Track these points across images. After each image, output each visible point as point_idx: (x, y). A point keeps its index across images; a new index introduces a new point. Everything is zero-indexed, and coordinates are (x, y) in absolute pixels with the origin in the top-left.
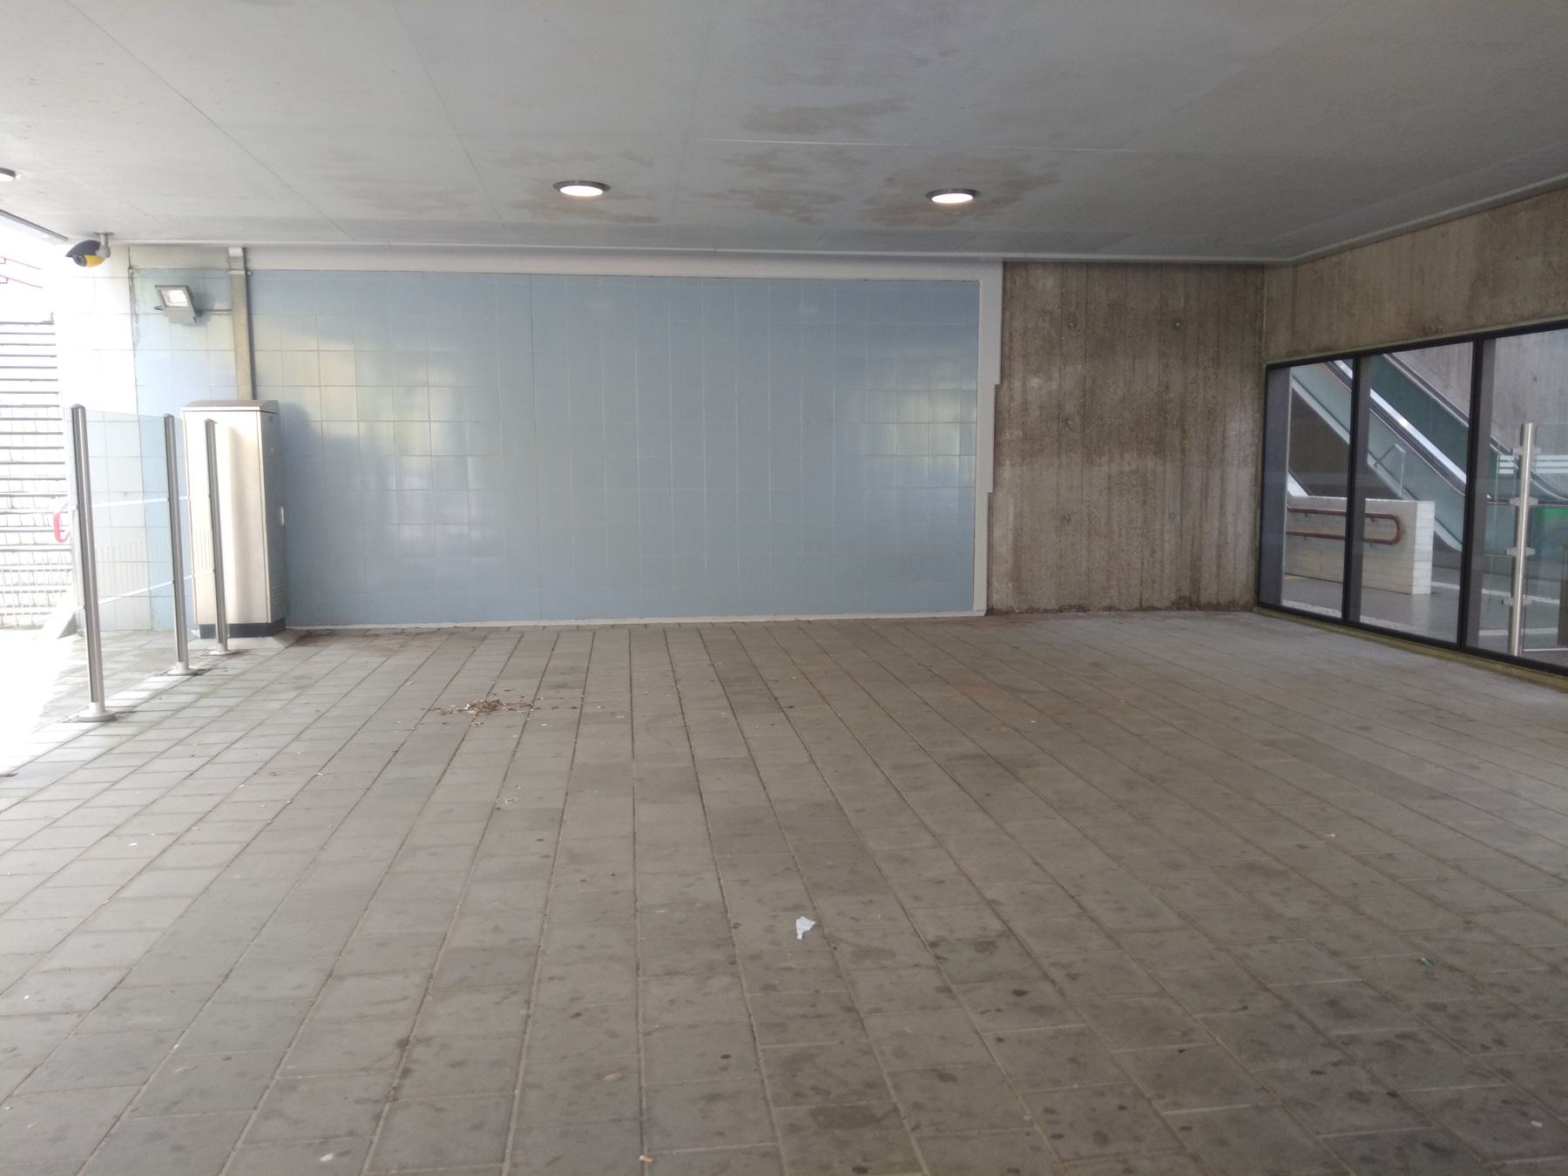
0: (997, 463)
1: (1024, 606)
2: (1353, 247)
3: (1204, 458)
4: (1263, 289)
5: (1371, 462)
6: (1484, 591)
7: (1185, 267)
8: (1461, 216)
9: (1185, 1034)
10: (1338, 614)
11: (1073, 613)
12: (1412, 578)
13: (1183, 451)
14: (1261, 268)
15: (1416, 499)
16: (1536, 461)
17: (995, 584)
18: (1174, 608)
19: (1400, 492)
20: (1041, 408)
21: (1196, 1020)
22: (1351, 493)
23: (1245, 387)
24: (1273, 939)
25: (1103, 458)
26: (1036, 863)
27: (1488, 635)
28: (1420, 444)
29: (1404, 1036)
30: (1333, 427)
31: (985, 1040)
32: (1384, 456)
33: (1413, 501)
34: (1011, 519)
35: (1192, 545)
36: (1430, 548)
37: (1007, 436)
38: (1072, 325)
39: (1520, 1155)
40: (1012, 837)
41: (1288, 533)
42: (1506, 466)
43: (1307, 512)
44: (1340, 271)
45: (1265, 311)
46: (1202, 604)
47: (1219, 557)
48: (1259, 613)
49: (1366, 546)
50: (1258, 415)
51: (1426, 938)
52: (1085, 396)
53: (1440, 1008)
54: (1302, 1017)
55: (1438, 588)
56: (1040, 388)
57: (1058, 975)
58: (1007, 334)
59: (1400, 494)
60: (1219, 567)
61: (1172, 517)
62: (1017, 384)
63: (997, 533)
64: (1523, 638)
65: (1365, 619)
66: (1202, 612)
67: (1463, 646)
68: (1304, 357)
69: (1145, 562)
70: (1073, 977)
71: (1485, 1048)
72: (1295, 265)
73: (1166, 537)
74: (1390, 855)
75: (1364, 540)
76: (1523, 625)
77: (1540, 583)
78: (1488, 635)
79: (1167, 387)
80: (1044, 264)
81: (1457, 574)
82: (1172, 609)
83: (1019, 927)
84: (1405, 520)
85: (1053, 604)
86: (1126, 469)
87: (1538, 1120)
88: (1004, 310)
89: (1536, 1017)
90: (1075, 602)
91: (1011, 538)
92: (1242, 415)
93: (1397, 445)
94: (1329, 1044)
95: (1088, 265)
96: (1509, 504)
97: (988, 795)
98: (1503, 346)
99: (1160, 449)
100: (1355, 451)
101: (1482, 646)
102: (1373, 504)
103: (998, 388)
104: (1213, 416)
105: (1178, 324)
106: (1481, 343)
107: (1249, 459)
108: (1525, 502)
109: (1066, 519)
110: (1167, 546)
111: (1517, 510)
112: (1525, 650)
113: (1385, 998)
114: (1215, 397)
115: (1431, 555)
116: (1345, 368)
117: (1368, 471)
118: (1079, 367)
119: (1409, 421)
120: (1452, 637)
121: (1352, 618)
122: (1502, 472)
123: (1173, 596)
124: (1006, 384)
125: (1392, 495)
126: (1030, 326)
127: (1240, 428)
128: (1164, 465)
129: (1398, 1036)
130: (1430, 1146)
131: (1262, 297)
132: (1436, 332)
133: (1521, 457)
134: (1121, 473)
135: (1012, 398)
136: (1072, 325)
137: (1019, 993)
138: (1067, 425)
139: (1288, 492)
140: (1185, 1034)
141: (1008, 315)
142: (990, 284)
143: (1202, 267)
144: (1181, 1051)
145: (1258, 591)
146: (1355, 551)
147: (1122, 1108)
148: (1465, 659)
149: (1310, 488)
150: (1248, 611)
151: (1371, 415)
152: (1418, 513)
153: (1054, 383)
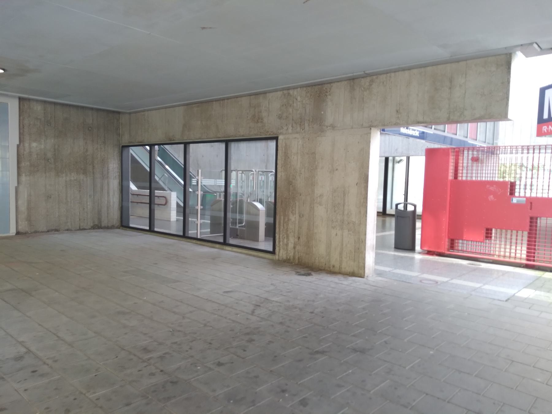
0: (19, 175)
1: (33, 230)
2: (148, 110)
3: (101, 176)
4: (119, 120)
5: (156, 177)
6: (190, 219)
7: (92, 109)
8: (179, 106)
9: (97, 370)
10: (148, 228)
11: (53, 232)
12: (170, 216)
13: (93, 173)
14: (119, 113)
15: (172, 191)
16: (202, 181)
17: (20, 223)
18: (92, 229)
19: (166, 189)
20: (37, 154)
21: (100, 365)
22: (150, 189)
23: (115, 152)
24: (126, 334)
25: (63, 174)
26: (40, 325)
27: (191, 232)
28: (171, 173)
29: (165, 354)
30: (144, 166)
31: (19, 392)
32: (161, 177)
33: (171, 192)
34: (26, 197)
35: (98, 206)
36: (175, 206)
37: (23, 164)
38: (49, 124)
39: (194, 377)
40: (30, 317)
41: (131, 202)
42: (194, 182)
43: (138, 195)
44: (144, 117)
45: (120, 127)
46: (102, 227)
47: (108, 210)
48: (122, 229)
49: (156, 206)
50: (119, 162)
51: (172, 324)
52: (55, 151)
53: (175, 343)
54: (135, 355)
55: (179, 219)
56: (36, 147)
57: (50, 362)
58: (21, 125)
59: (167, 190)
60: (108, 213)
61: (90, 196)
62: (27, 145)
63: (20, 202)
64: (200, 233)
65: (156, 229)
66: (102, 230)
67: (184, 236)
68: (133, 144)
69: (81, 213)
70: (56, 361)
71: (187, 351)
72: (130, 113)
73: (88, 204)
74: (162, 301)
75: (542, 197)
76: (200, 229)
77: (206, 216)
78: (191, 232)
79: (87, 150)
80: (37, 101)
81: (182, 214)
82: (91, 229)
83: (33, 349)
84: (168, 198)
85: (45, 229)
86: (72, 179)
87: (199, 366)
88: (20, 116)
89: (200, 339)
90: (53, 228)
91: (26, 204)
92: (114, 162)
93: (165, 174)
94: (144, 361)
95: (55, 104)
96: (195, 193)
97: (19, 303)
98: (192, 146)
99: (85, 172)
100: (151, 174)
101: (190, 236)
102: (158, 193)
103: (18, 146)
104: (104, 162)
105: (90, 129)
106: (186, 145)
107: (117, 177)
108: (200, 193)
109: (49, 197)
110: (89, 207)
111: (198, 195)
112: (201, 236)
113: (160, 344)
114: (104, 155)
115: (176, 209)
116: (148, 148)
117: (157, 182)
118: (53, 141)
119: (169, 167)
120: (181, 234)
121: (152, 229)
122: (193, 184)
123: (92, 225)
124: (22, 144)
125: (164, 190)
126: (31, 123)
127: (113, 166)
128: (87, 178)
129: (164, 354)
130: (172, 382)
131: (119, 123)
132: (173, 140)
133: (198, 179)
134: (70, 180)
135: (24, 150)
136: (49, 124)
137: (33, 372)
138: (49, 162)
139: (131, 188)
140: (97, 370)
141: (21, 118)
142: (13, 107)
143: (98, 110)
144: (96, 376)
145: (122, 221)
146: (152, 208)
147: (75, 399)
148: (185, 240)
149: (138, 187)
150: (118, 228)
151: (155, 163)
152: (172, 196)
153: (42, 146)
